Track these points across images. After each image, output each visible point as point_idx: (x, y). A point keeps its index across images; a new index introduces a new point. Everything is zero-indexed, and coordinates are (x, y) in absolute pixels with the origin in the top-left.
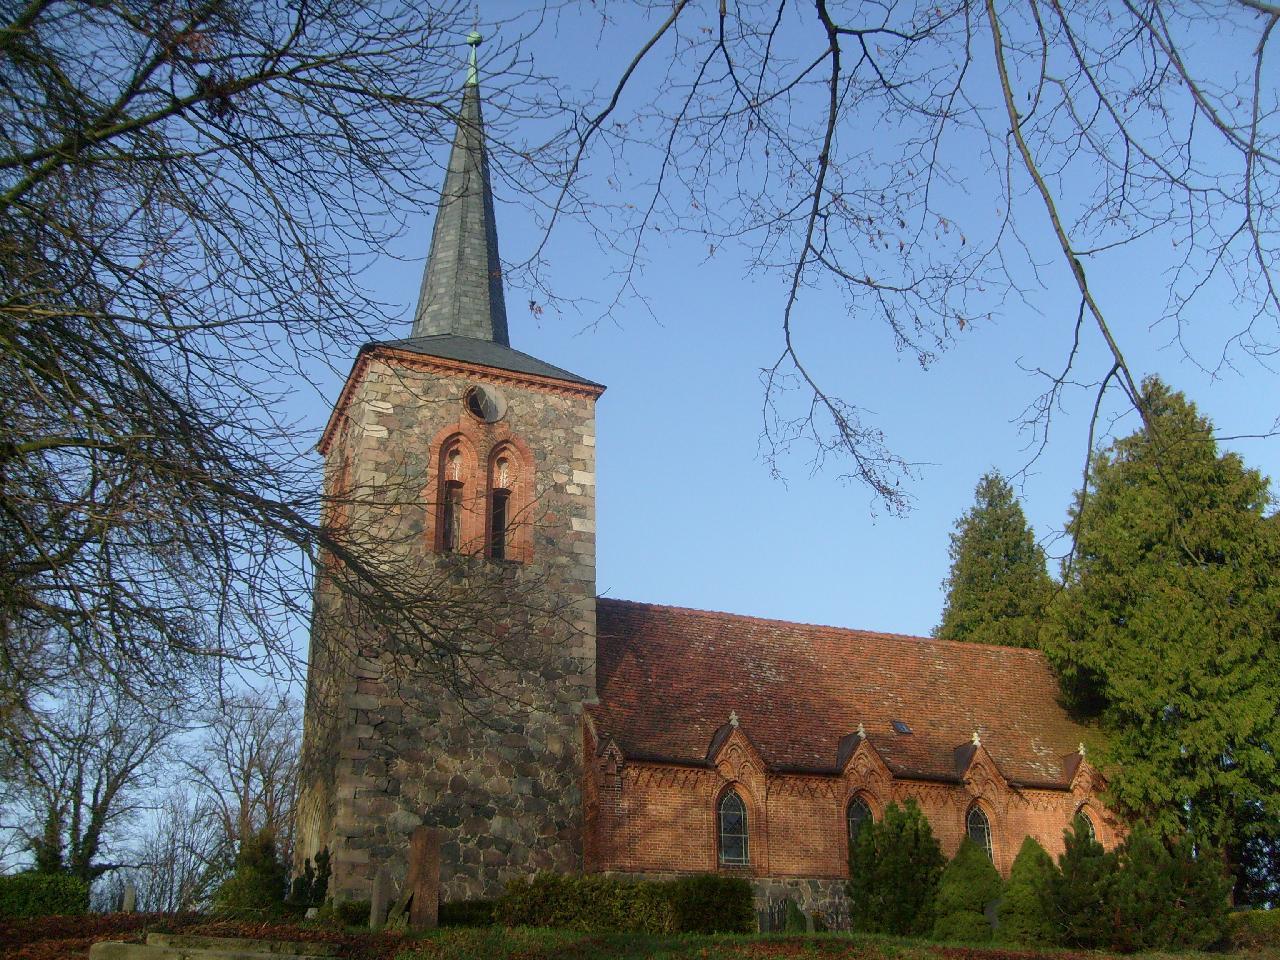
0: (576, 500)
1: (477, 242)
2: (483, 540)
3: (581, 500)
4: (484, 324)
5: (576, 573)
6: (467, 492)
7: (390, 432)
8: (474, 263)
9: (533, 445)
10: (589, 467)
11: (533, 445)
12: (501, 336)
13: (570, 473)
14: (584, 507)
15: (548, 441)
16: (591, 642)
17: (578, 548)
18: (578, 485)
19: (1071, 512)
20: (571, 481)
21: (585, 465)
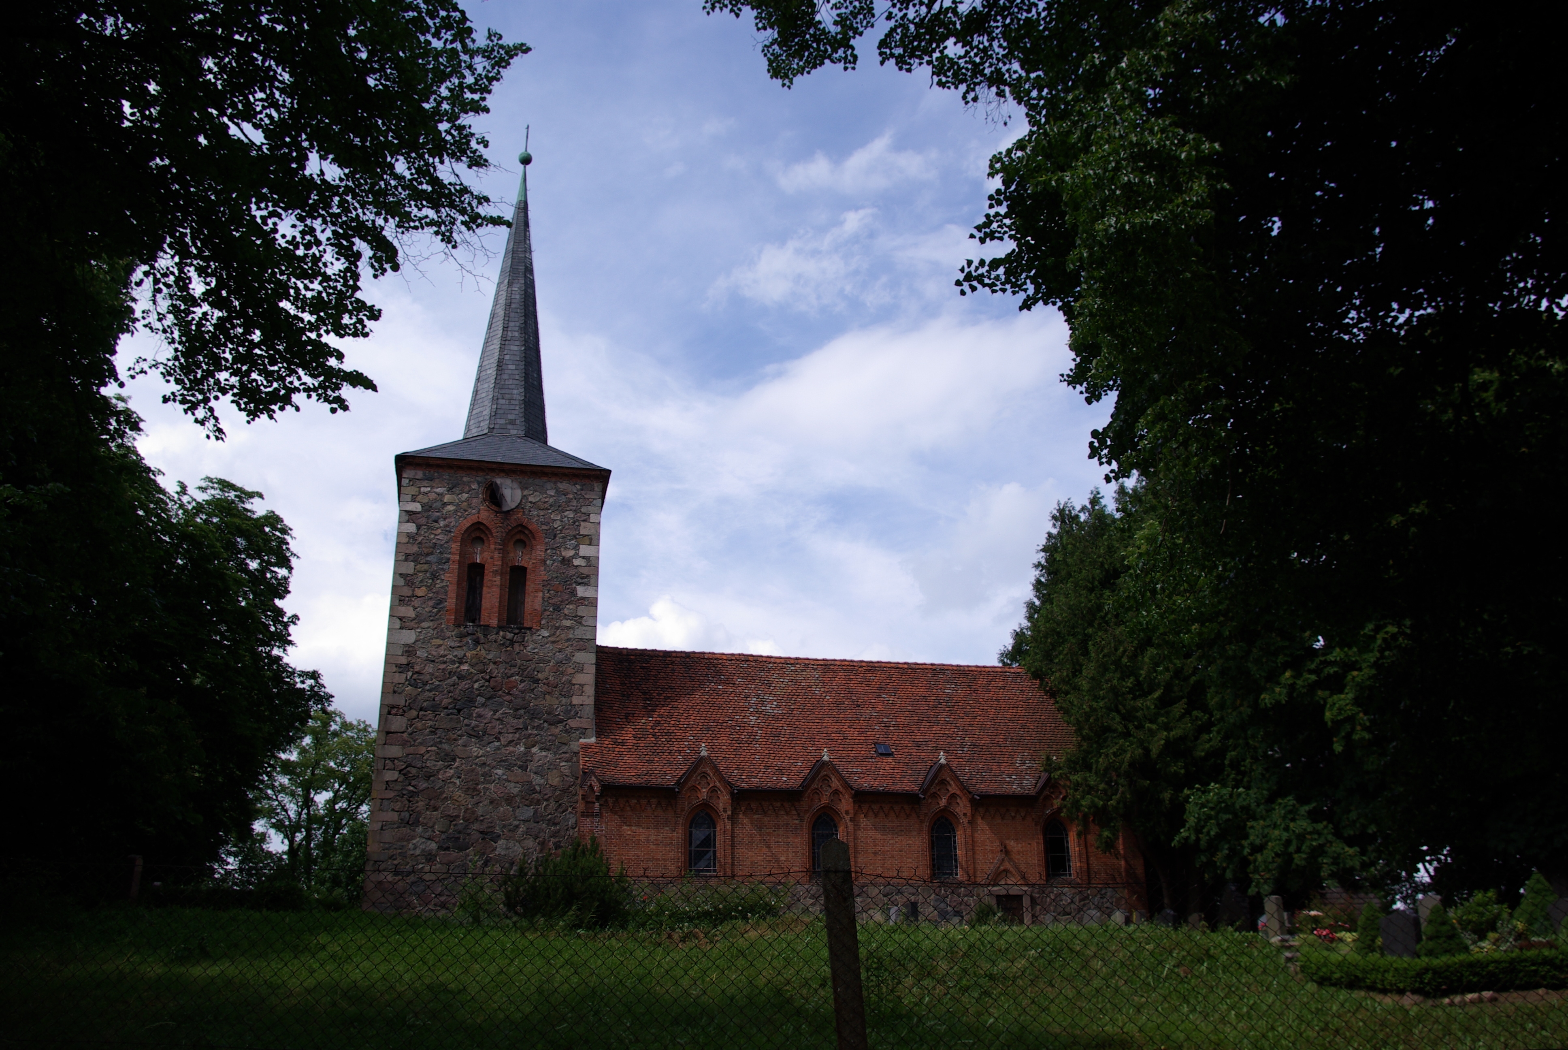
0: (581, 570)
1: (516, 348)
2: (827, 992)
3: (585, 571)
4: (518, 422)
5: (579, 633)
6: (488, 569)
7: (419, 528)
8: (512, 367)
9: (544, 527)
10: (594, 542)
11: (544, 527)
12: (536, 429)
13: (576, 548)
14: (588, 576)
15: (559, 523)
16: (590, 690)
17: (582, 611)
18: (584, 557)
19: (1038, 565)
20: (576, 556)
21: (591, 540)
